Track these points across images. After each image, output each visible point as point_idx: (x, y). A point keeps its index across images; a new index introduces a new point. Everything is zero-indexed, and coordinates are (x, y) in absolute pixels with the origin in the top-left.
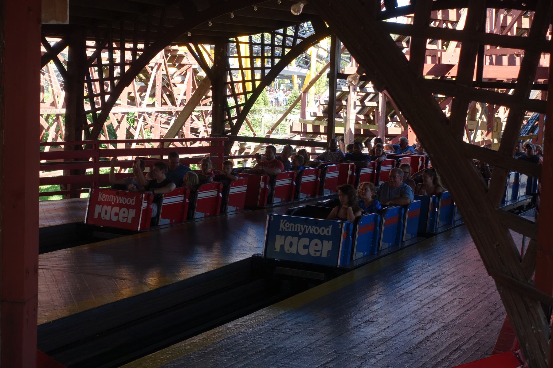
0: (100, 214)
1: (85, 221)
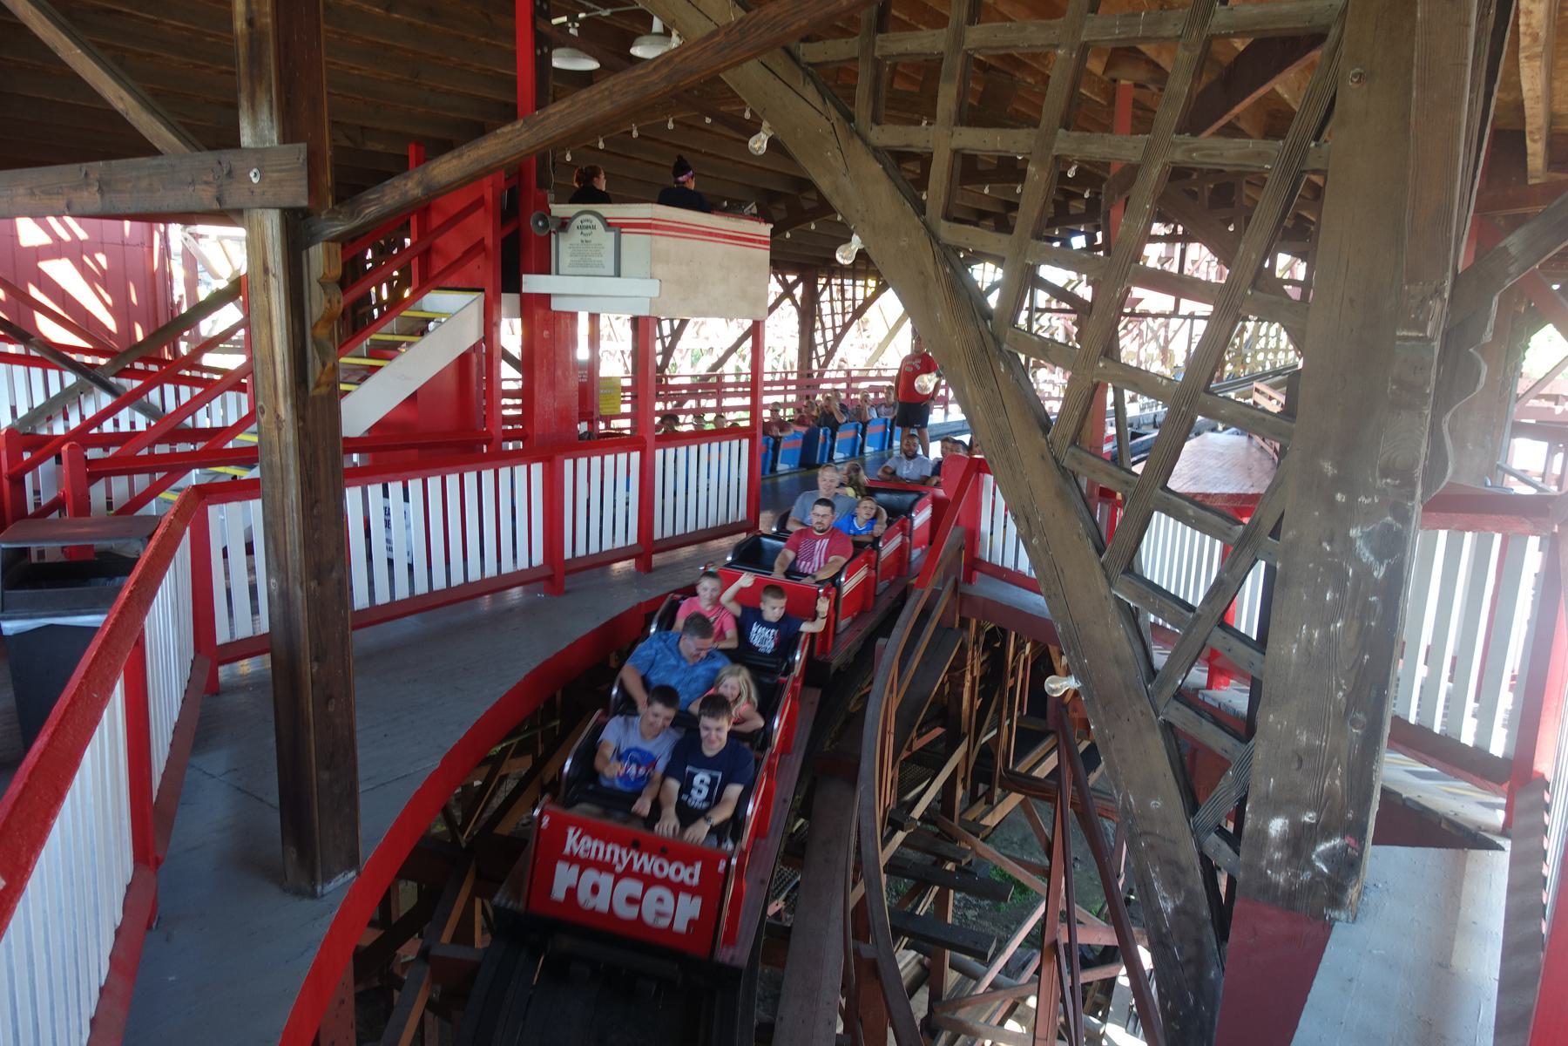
0: (572, 892)
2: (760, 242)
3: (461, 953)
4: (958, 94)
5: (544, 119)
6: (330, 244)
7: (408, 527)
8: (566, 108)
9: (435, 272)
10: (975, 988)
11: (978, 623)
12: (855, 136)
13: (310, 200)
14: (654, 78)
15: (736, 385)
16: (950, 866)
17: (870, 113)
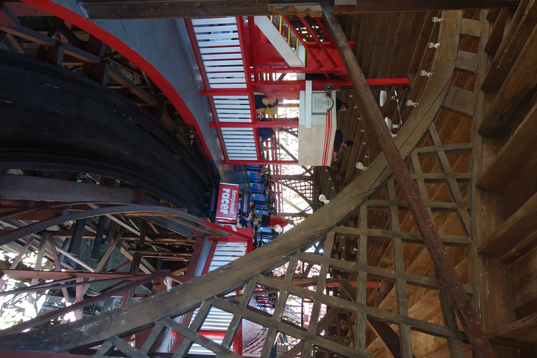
0: (225, 192)
1: (222, 183)
2: (324, 163)
3: (60, 58)
4: (378, 236)
5: (367, 90)
6: (322, 13)
7: (223, 40)
8: (371, 98)
9: (312, 50)
10: (59, 247)
11: (195, 243)
12: (363, 200)
13: (337, 6)
14: (382, 130)
15: (276, 154)
16: (104, 237)
17: (371, 205)
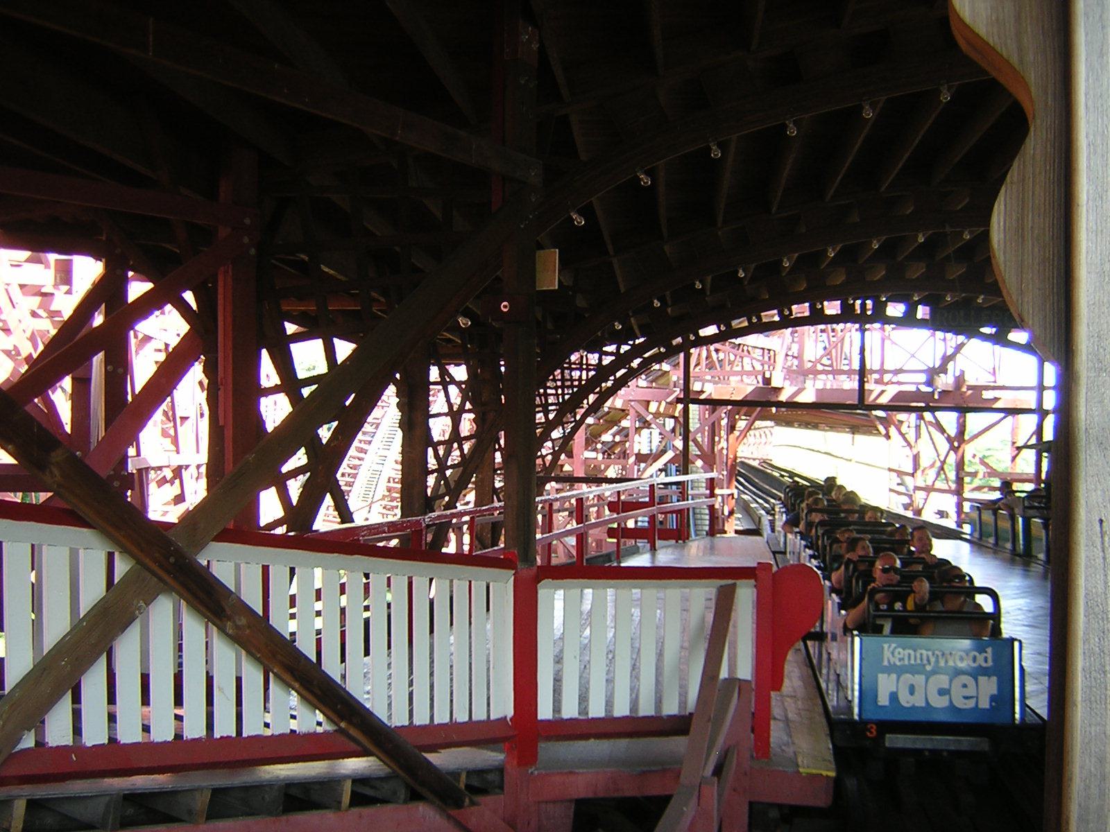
0: (894, 697)
